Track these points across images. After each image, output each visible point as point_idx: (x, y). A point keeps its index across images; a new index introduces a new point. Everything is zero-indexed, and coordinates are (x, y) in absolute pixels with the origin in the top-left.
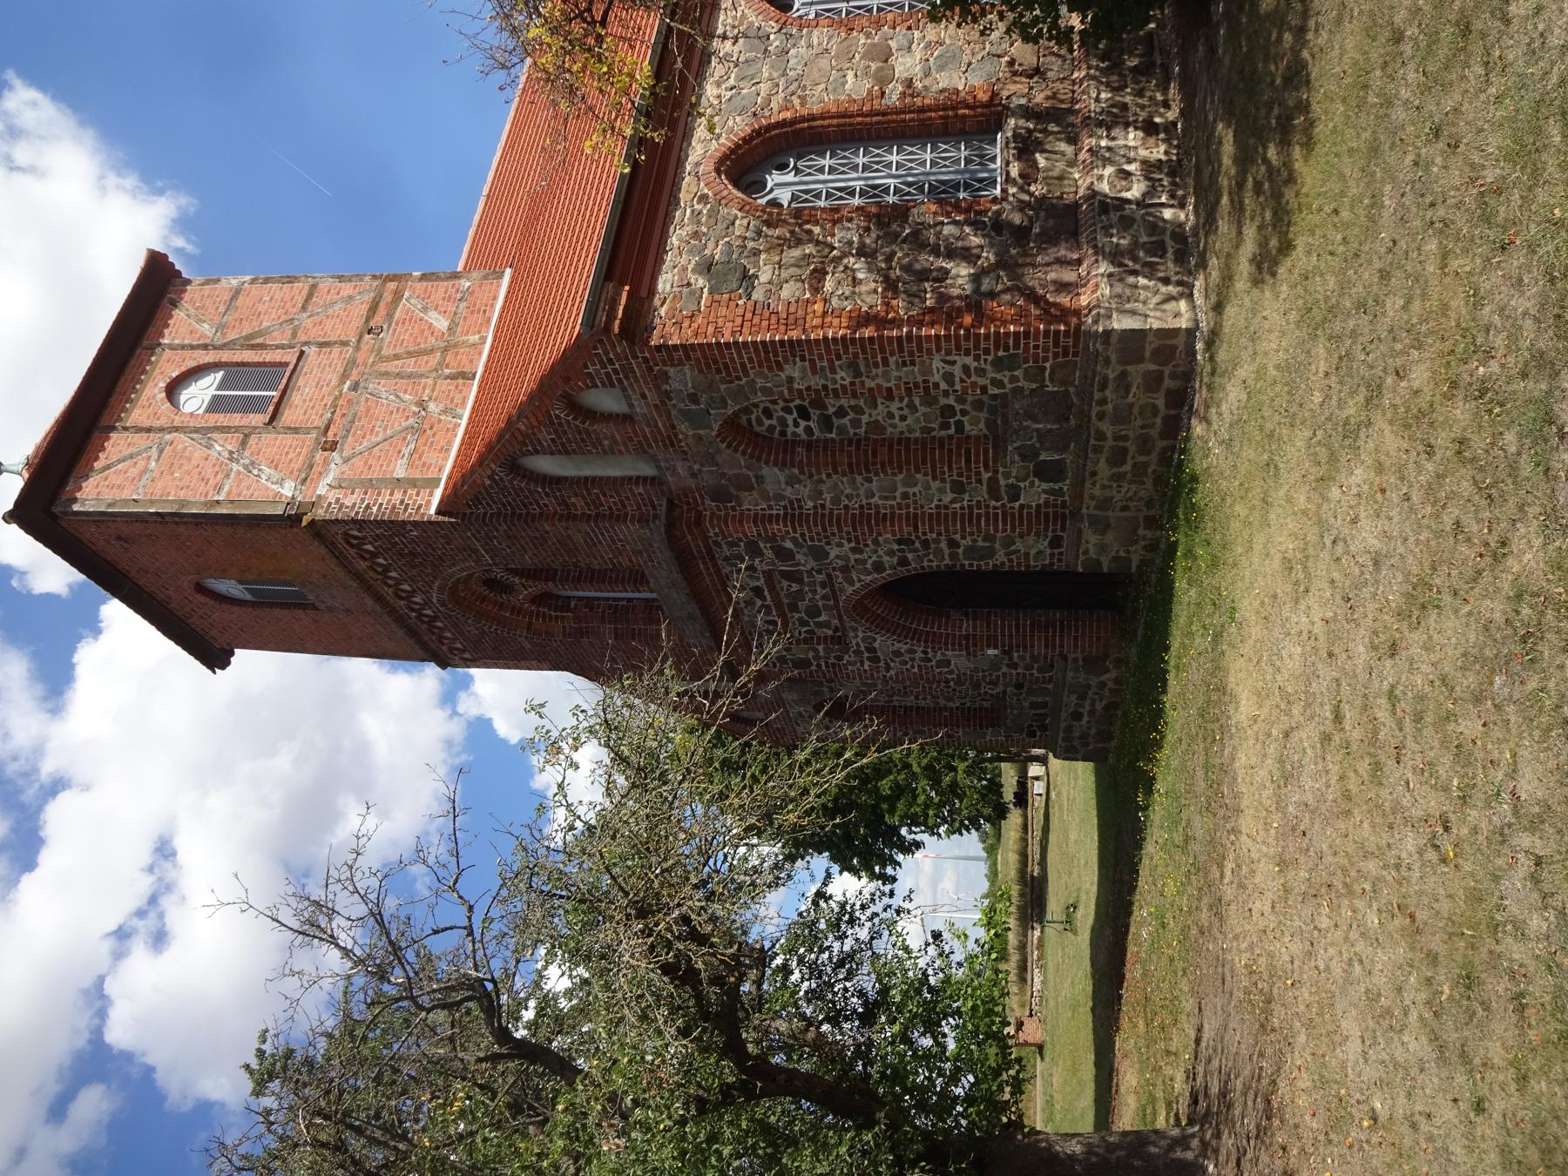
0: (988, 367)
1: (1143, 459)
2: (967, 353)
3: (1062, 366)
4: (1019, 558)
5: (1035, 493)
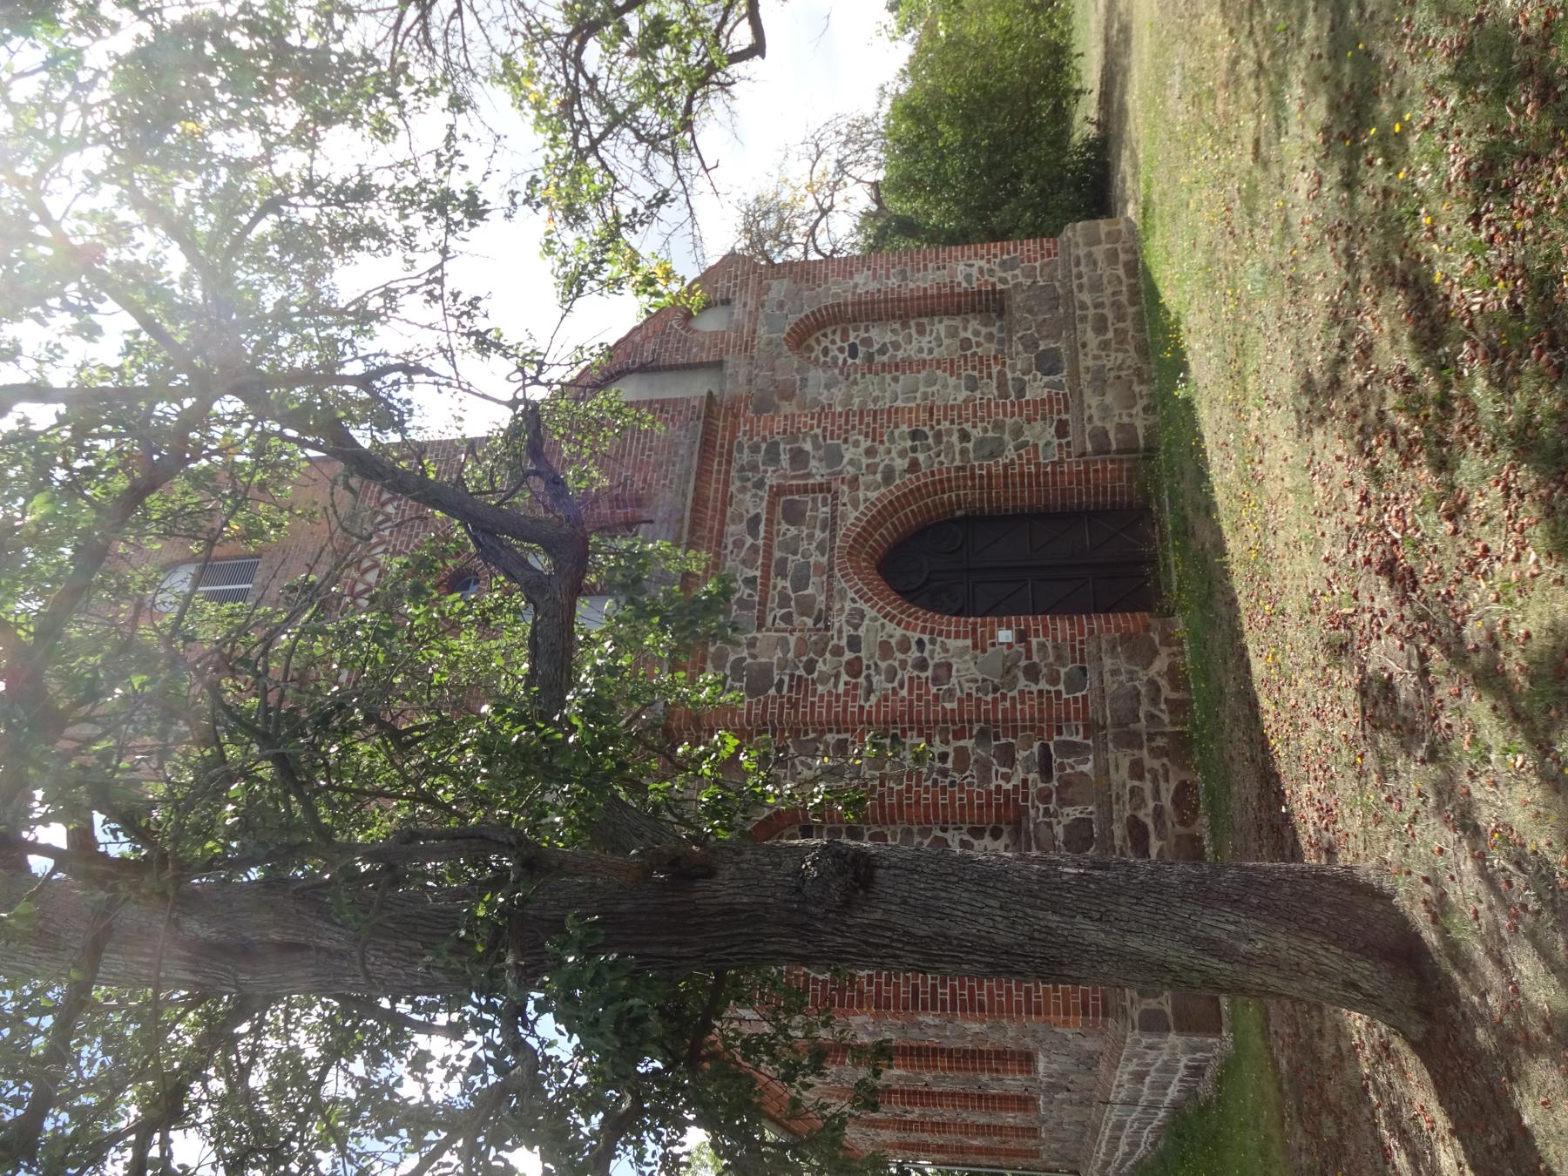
0: (996, 268)
1: (1121, 325)
2: (982, 257)
3: (1048, 264)
4: (1028, 453)
5: (1037, 389)
